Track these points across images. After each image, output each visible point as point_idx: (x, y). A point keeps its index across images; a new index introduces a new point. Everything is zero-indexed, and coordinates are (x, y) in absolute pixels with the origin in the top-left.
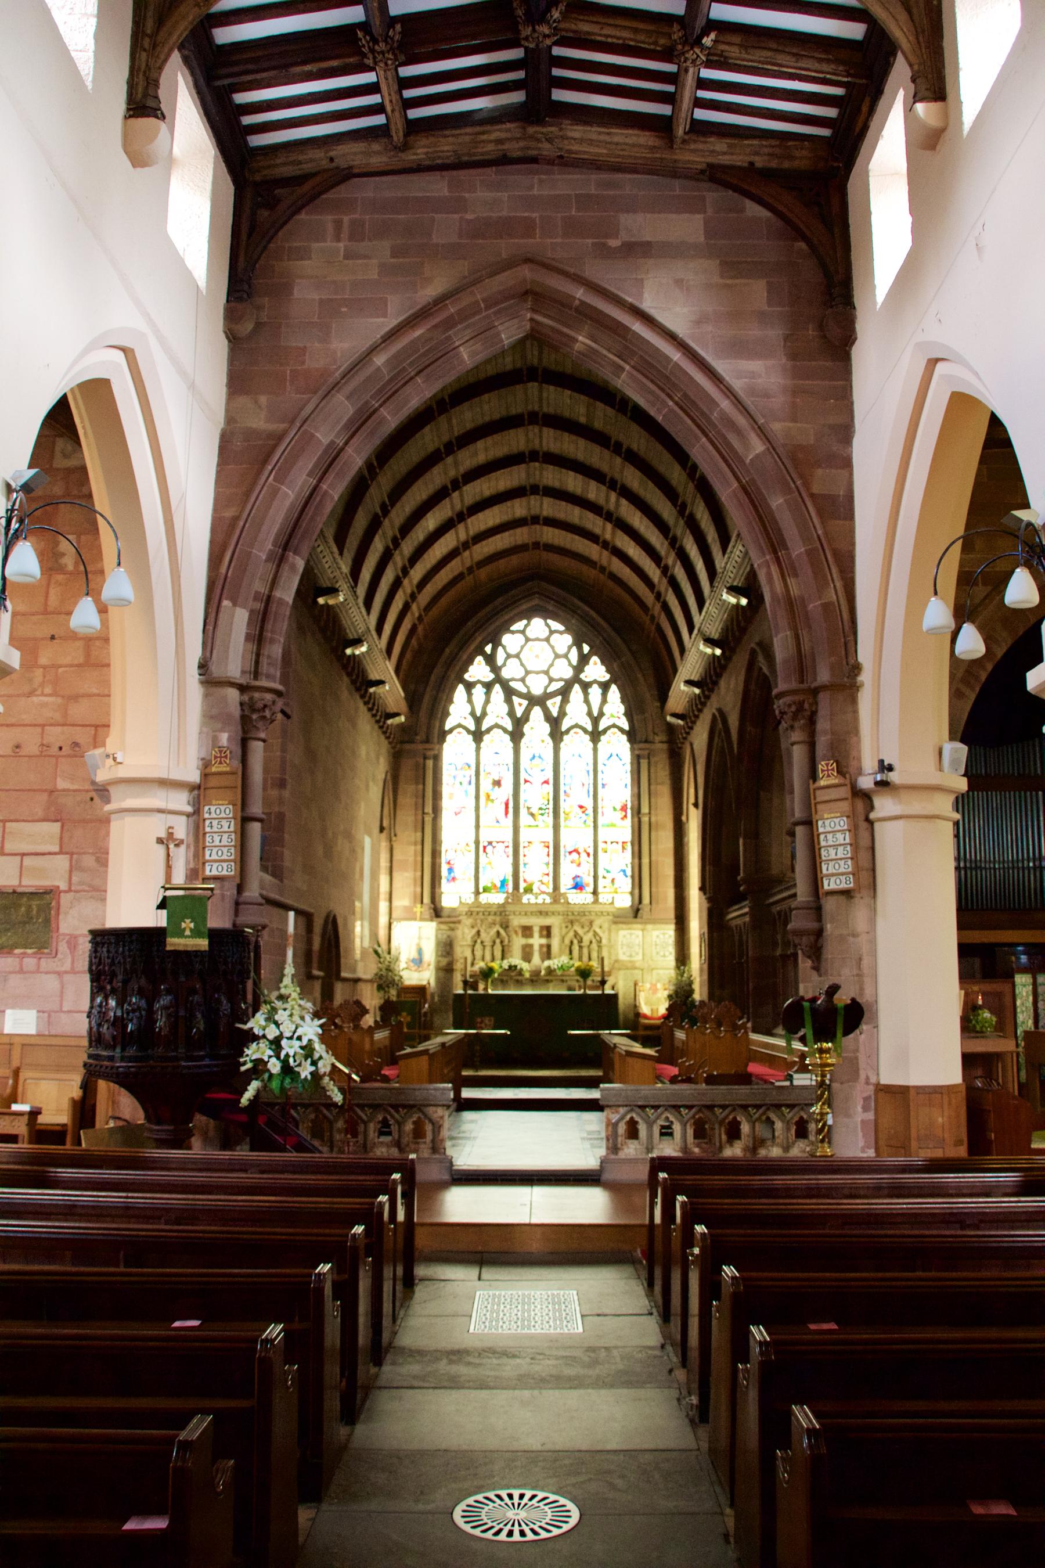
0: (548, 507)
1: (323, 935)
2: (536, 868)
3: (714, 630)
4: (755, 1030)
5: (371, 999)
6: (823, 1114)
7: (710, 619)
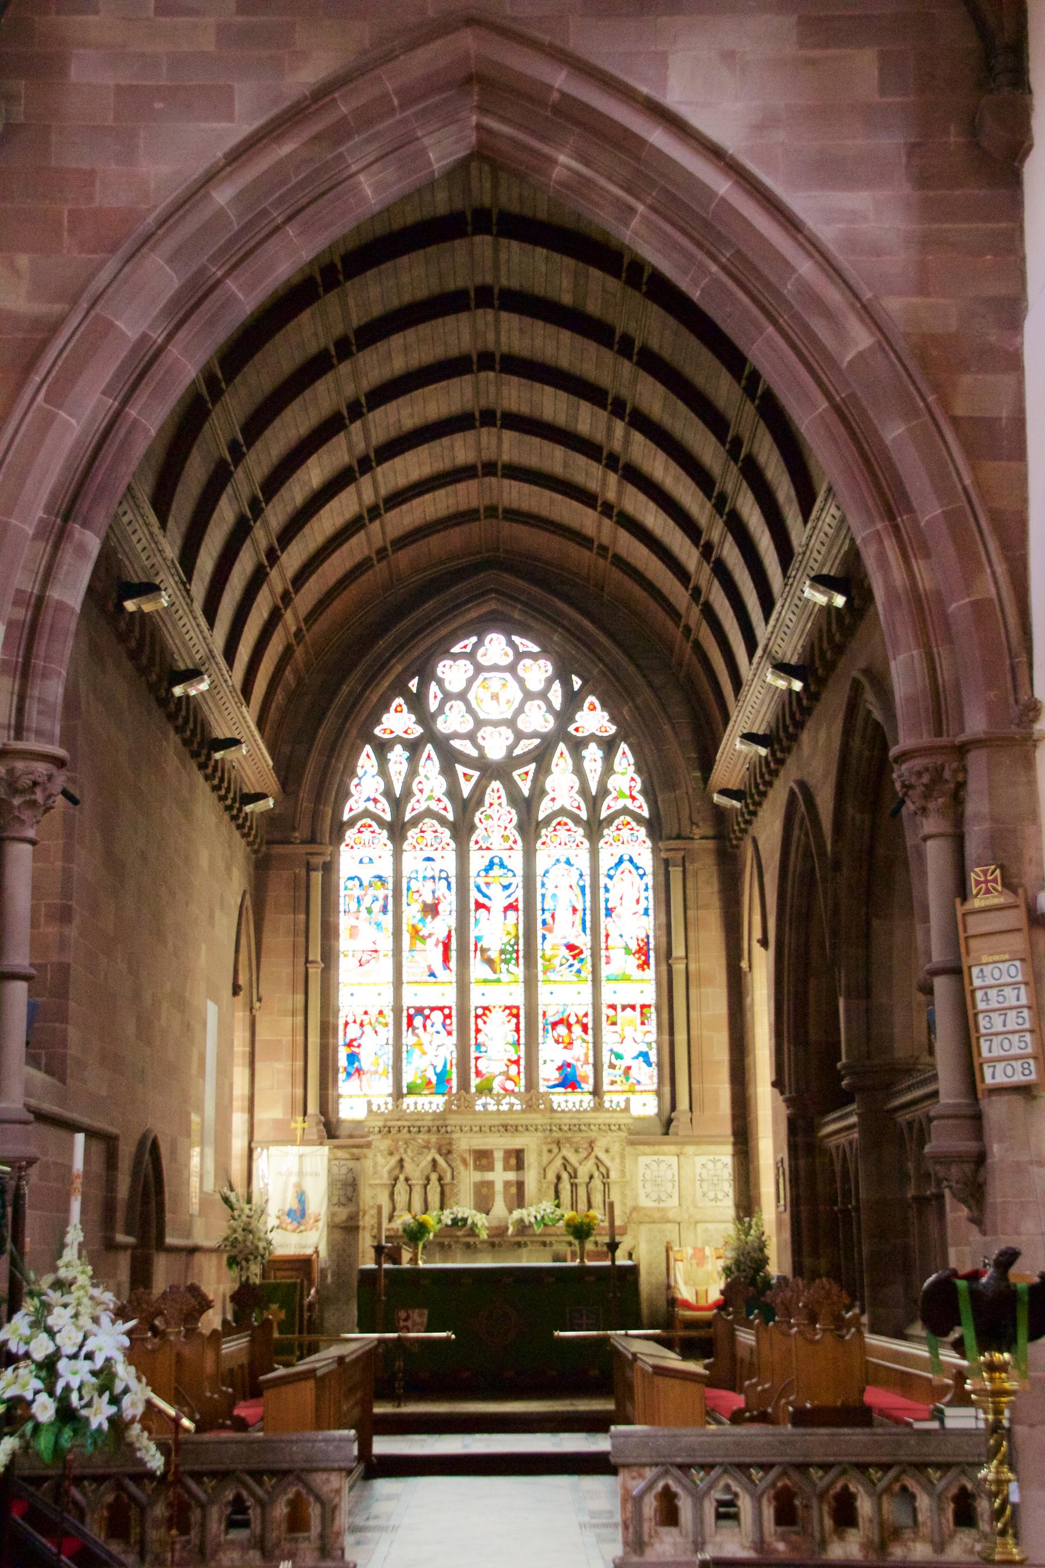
0: (512, 447)
1: (135, 1174)
2: (497, 1045)
3: (790, 650)
4: (876, 1329)
5: (217, 1283)
6: (1000, 1483)
7: (785, 633)
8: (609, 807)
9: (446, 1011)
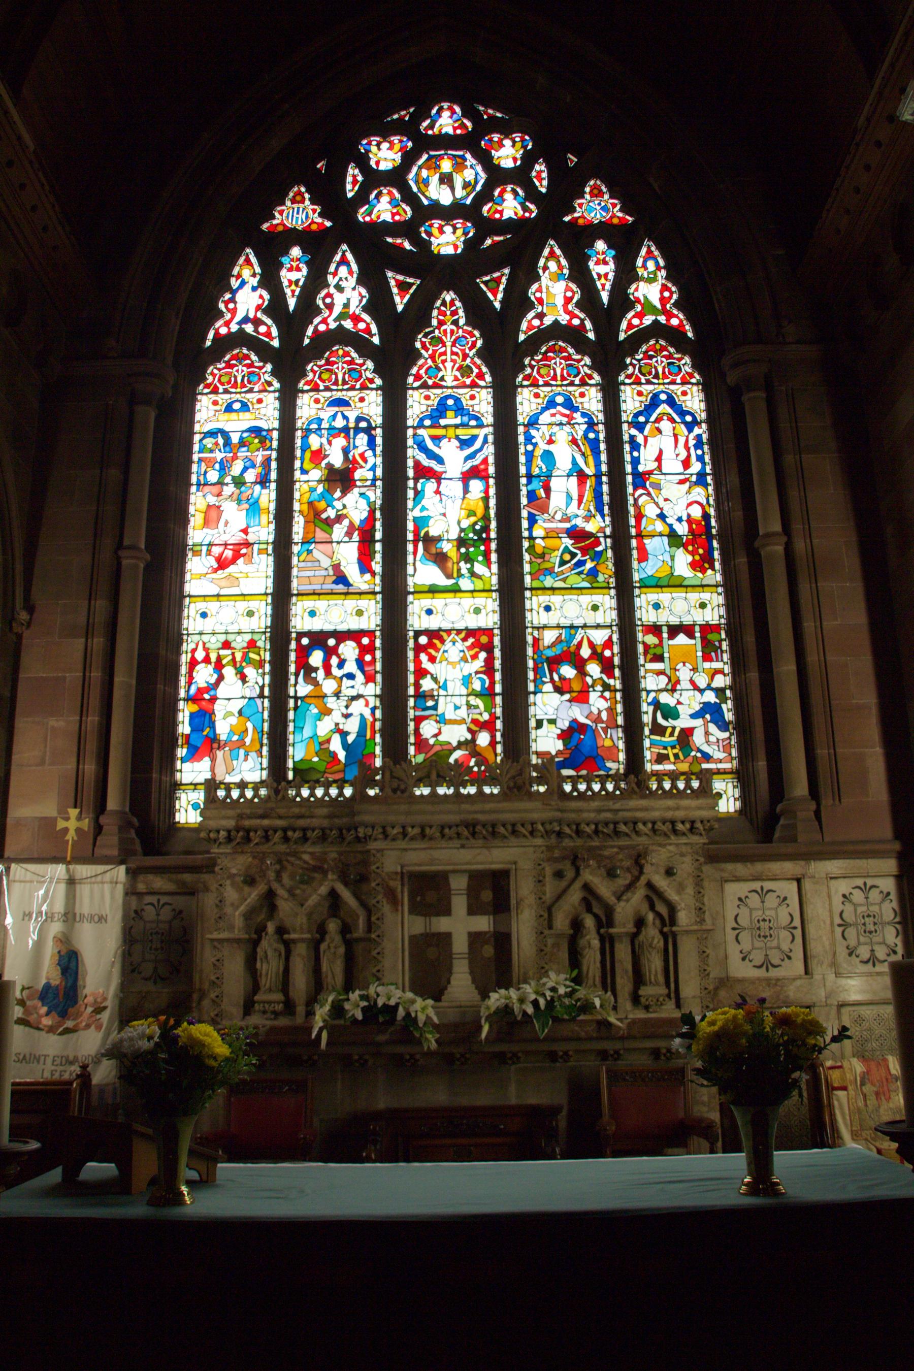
2: (454, 700)
8: (630, 326)
9: (365, 641)
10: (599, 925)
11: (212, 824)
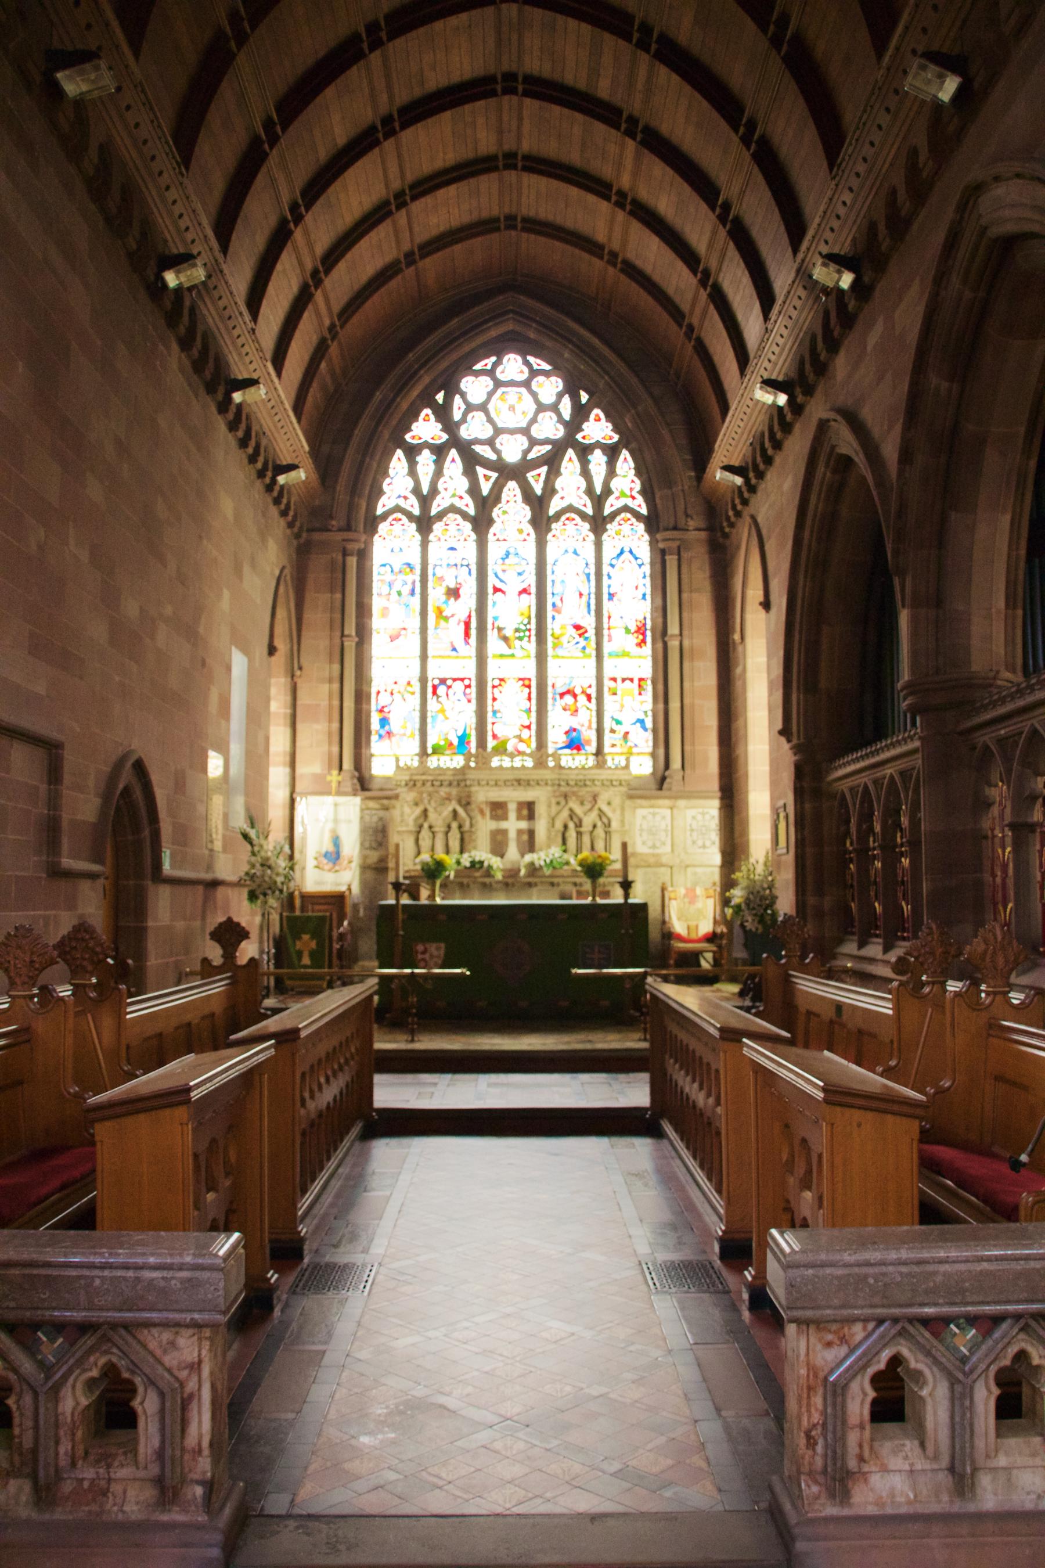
2: (511, 715)
9: (467, 682)
10: (576, 826)
11: (399, 778)
